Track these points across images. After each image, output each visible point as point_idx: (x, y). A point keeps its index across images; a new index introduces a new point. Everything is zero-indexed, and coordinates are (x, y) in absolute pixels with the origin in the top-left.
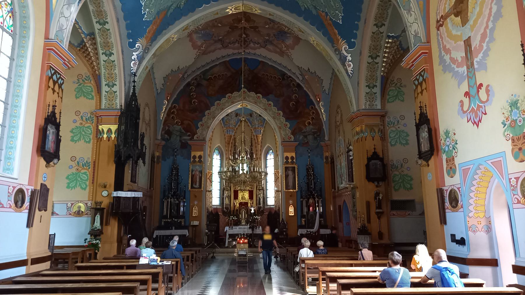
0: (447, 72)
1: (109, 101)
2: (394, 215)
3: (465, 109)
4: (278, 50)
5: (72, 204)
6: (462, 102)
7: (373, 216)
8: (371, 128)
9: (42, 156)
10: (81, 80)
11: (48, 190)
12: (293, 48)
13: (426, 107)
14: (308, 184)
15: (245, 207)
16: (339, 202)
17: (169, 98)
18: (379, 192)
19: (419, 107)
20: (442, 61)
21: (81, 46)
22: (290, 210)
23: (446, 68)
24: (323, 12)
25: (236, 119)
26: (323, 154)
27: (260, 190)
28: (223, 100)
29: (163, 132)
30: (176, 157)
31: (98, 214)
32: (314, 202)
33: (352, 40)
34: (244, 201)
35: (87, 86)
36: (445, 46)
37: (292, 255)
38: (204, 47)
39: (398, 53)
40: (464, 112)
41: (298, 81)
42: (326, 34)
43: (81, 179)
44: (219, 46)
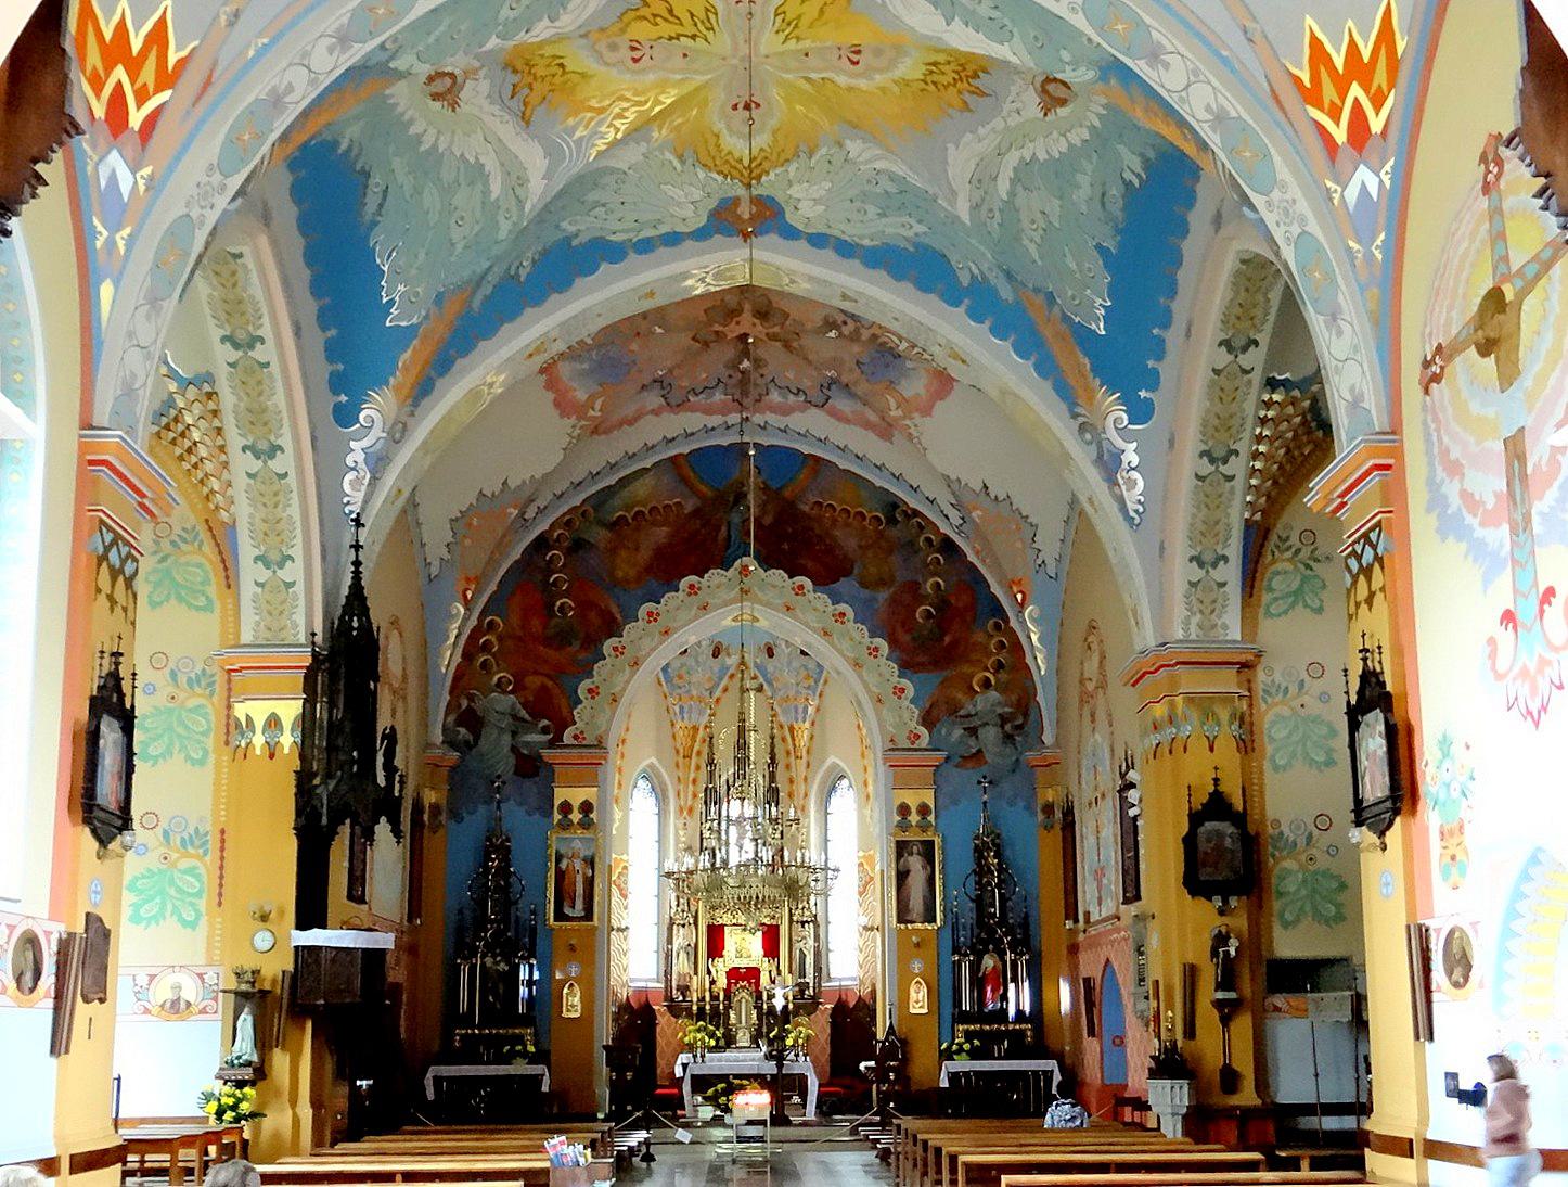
0: (1451, 540)
1: (267, 616)
2: (1277, 1009)
3: (1502, 667)
4: (873, 417)
5: (152, 977)
6: (1492, 642)
7: (1207, 1016)
8: (1203, 704)
9: (87, 821)
10: (165, 544)
11: (106, 934)
12: (927, 411)
13: (1380, 653)
14: (981, 903)
15: (750, 984)
16: (1090, 966)
17: (469, 594)
18: (1228, 933)
19: (1360, 651)
20: (1437, 502)
21: (164, 420)
22: (913, 994)
23: (1450, 527)
24: (1037, 290)
25: (715, 664)
26: (1034, 795)
27: (803, 923)
28: (670, 600)
29: (451, 719)
30: (499, 808)
31: (246, 1010)
32: (1000, 965)
33: (1143, 394)
34: (743, 963)
35: (187, 564)
36: (1447, 451)
37: (915, 1144)
38: (598, 406)
39: (1305, 438)
40: (1499, 677)
41: (944, 528)
42: (1046, 368)
43: (180, 890)
44: (654, 399)
